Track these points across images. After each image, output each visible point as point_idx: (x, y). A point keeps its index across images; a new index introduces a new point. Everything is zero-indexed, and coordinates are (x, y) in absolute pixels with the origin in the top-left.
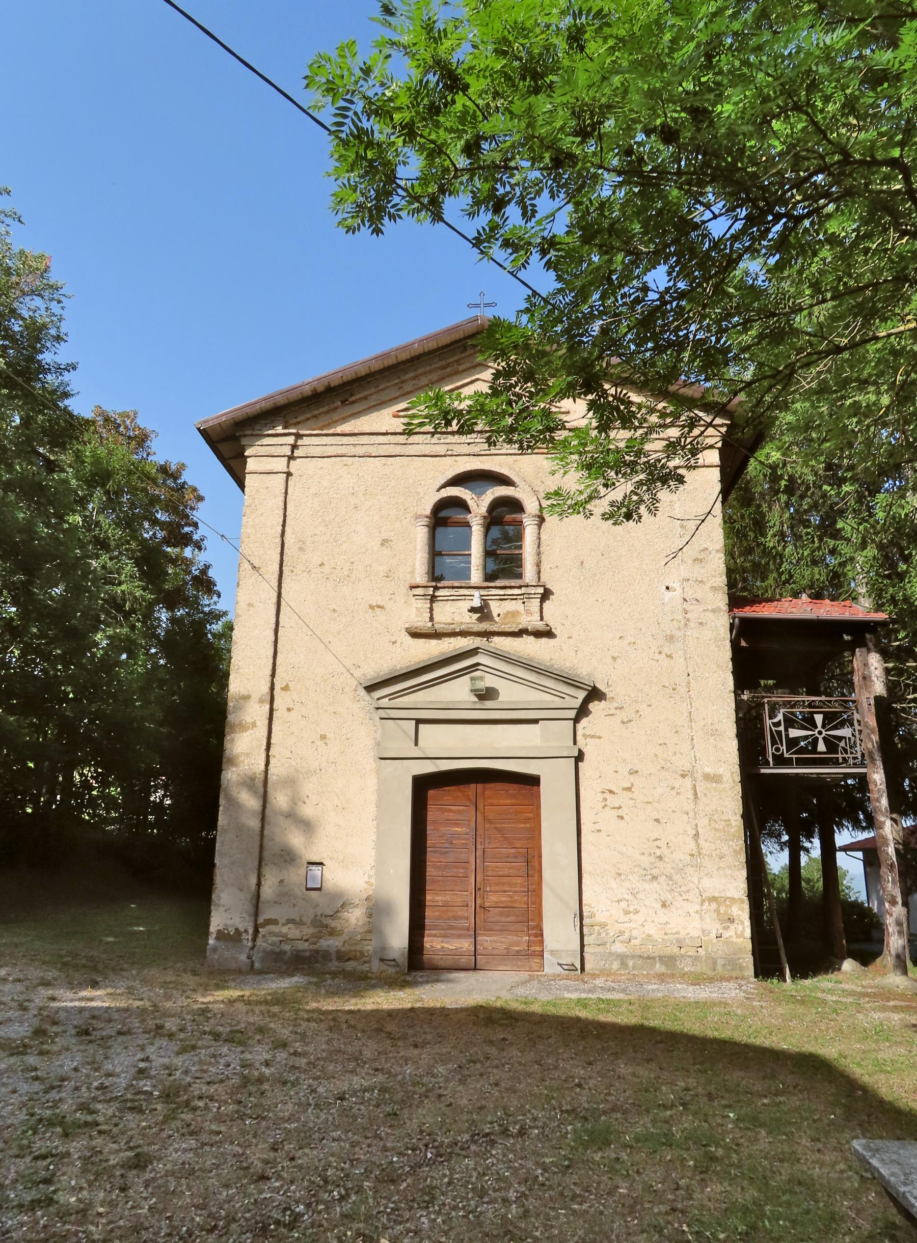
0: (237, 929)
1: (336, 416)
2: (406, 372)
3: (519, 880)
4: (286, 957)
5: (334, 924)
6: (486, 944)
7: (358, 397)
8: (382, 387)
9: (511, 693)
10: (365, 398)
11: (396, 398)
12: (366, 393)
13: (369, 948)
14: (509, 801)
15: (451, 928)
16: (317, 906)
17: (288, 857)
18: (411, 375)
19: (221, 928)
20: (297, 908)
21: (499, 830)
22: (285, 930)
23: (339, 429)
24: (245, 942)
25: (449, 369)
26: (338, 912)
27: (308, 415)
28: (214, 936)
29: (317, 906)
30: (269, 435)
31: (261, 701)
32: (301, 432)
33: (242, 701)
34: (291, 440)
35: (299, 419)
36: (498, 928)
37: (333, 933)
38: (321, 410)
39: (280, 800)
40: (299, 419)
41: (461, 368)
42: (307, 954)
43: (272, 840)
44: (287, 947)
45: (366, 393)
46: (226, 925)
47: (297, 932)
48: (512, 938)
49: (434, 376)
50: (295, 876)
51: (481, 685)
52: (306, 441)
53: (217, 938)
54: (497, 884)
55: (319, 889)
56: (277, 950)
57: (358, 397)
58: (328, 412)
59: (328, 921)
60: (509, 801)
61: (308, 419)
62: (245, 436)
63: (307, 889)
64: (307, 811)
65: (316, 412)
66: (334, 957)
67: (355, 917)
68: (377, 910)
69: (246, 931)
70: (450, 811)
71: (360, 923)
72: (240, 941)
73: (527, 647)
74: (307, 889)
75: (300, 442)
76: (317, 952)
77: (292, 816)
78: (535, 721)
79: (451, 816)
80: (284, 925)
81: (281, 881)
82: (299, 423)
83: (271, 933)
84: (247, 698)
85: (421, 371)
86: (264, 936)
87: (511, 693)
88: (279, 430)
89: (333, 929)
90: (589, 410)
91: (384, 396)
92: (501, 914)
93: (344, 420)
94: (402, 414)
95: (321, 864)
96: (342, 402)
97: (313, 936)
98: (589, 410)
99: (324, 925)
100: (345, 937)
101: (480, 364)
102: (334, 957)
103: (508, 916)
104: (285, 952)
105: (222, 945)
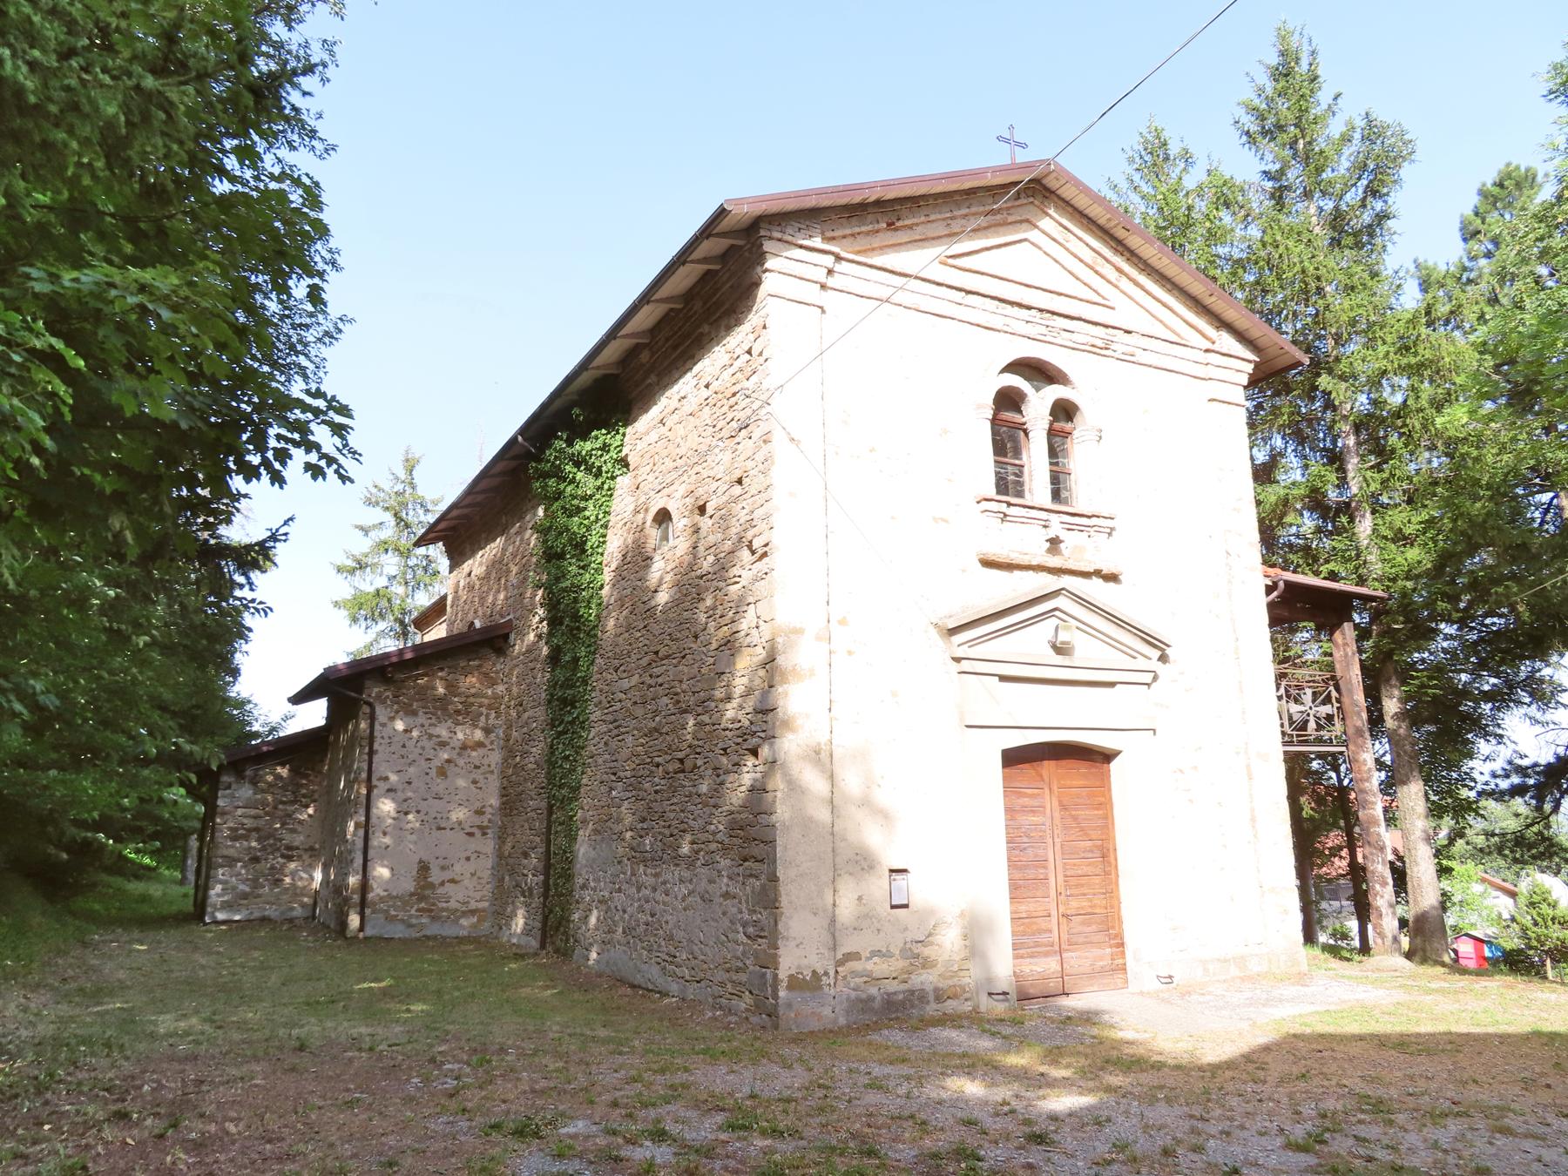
0: (814, 972)
1: (876, 241)
2: (958, 205)
3: (1097, 880)
4: (877, 1004)
5: (926, 951)
6: (1072, 962)
7: (907, 222)
8: (932, 217)
9: (1090, 652)
10: (910, 227)
11: (940, 237)
12: (915, 220)
13: (970, 979)
14: (1081, 783)
15: (1037, 945)
16: (906, 929)
17: (863, 862)
18: (964, 211)
19: (793, 972)
20: (882, 934)
21: (1075, 818)
22: (869, 966)
23: (878, 260)
24: (826, 989)
25: (999, 217)
26: (930, 935)
27: (848, 231)
28: (785, 984)
29: (906, 929)
30: (801, 247)
31: (818, 638)
32: (843, 254)
33: (793, 637)
34: (829, 261)
35: (836, 234)
36: (1081, 940)
37: (927, 964)
38: (864, 229)
39: (851, 782)
40: (836, 234)
41: (1010, 219)
42: (901, 997)
43: (844, 840)
44: (873, 991)
45: (915, 220)
46: (799, 967)
47: (885, 966)
48: (1097, 952)
49: (982, 221)
50: (877, 887)
51: (1063, 636)
52: (843, 267)
53: (790, 987)
54: (1077, 886)
55: (906, 906)
56: (864, 996)
57: (907, 222)
58: (868, 233)
59: (917, 949)
60: (1081, 783)
61: (844, 237)
62: (771, 238)
63: (893, 907)
64: (882, 798)
65: (857, 230)
66: (931, 998)
67: (949, 942)
68: (975, 933)
69: (826, 974)
70: (1026, 795)
71: (956, 948)
72: (820, 988)
73: (1094, 589)
74: (893, 907)
75: (838, 267)
76: (912, 992)
77: (865, 803)
78: (1112, 685)
79: (1025, 801)
80: (868, 959)
81: (860, 898)
82: (834, 238)
83: (855, 974)
84: (798, 631)
85: (974, 209)
86: (845, 978)
87: (1090, 652)
88: (817, 242)
89: (925, 959)
90: (1047, 214)
91: (932, 230)
92: (1083, 923)
93: (883, 248)
94: (950, 261)
95: (905, 871)
96: (889, 225)
97: (904, 971)
98: (1047, 214)
99: (916, 957)
100: (940, 969)
101: (1027, 221)
102: (931, 998)
103: (1089, 925)
104: (871, 999)
105: (797, 997)
